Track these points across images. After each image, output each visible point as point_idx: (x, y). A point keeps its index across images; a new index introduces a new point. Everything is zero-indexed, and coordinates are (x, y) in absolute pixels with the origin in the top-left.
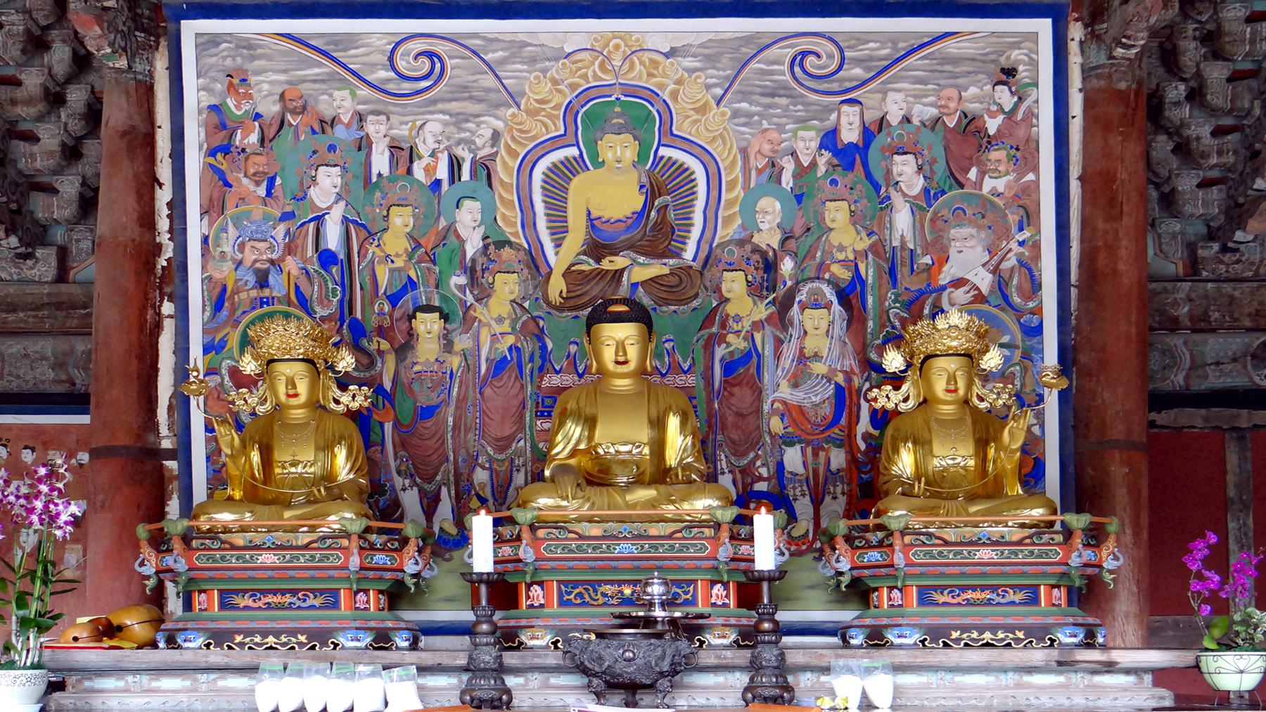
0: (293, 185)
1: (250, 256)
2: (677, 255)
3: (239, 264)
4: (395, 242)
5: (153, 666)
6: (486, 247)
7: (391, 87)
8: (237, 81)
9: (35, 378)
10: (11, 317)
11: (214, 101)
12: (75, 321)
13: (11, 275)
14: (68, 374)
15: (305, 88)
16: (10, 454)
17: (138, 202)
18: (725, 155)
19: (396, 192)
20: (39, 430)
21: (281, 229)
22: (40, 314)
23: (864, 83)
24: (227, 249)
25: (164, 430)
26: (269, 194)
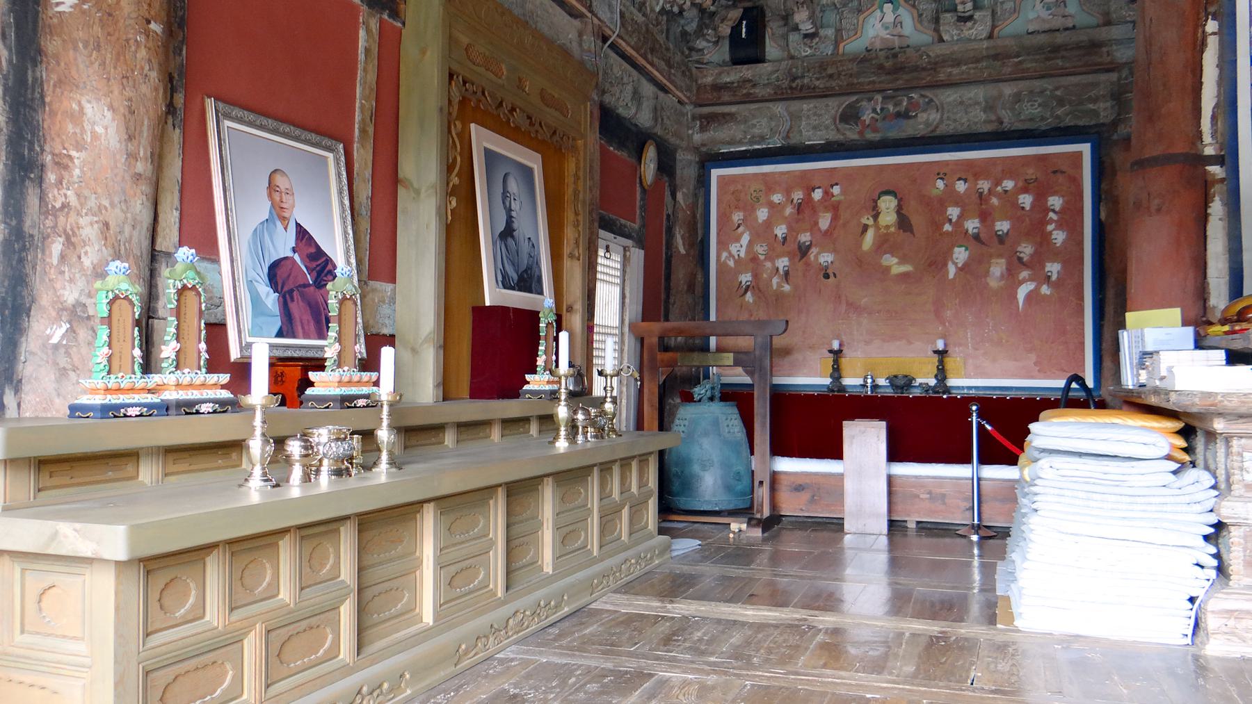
17: (37, 12)
20: (969, 163)
22: (980, 65)
25: (1207, 138)
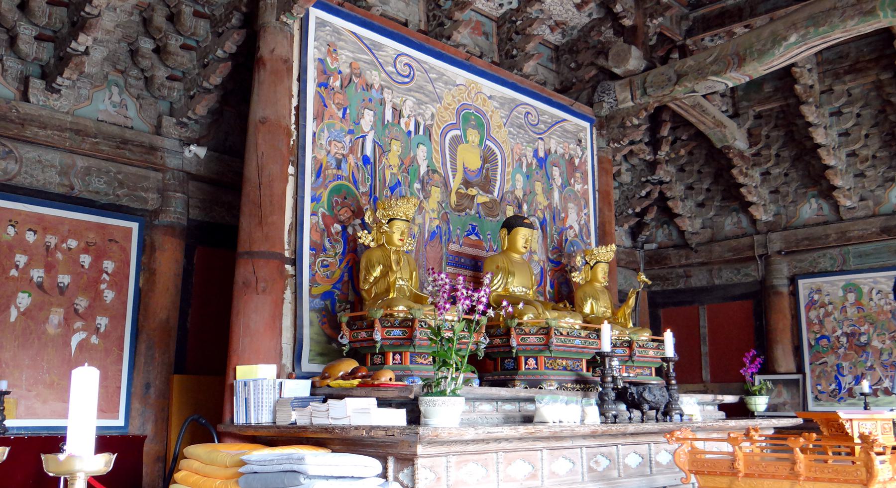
0: (354, 115)
1: (334, 151)
2: (492, 194)
3: (329, 152)
4: (393, 159)
5: (490, 397)
6: (428, 171)
7: (393, 76)
8: (332, 50)
9: (45, 179)
10: (42, 133)
11: (321, 57)
12: (88, 146)
13: (38, 101)
14: (70, 181)
15: (361, 64)
16: (17, 233)
18: (507, 152)
19: (394, 131)
20: (41, 217)
21: (348, 138)
23: (545, 132)
24: (324, 143)
26: (344, 117)
